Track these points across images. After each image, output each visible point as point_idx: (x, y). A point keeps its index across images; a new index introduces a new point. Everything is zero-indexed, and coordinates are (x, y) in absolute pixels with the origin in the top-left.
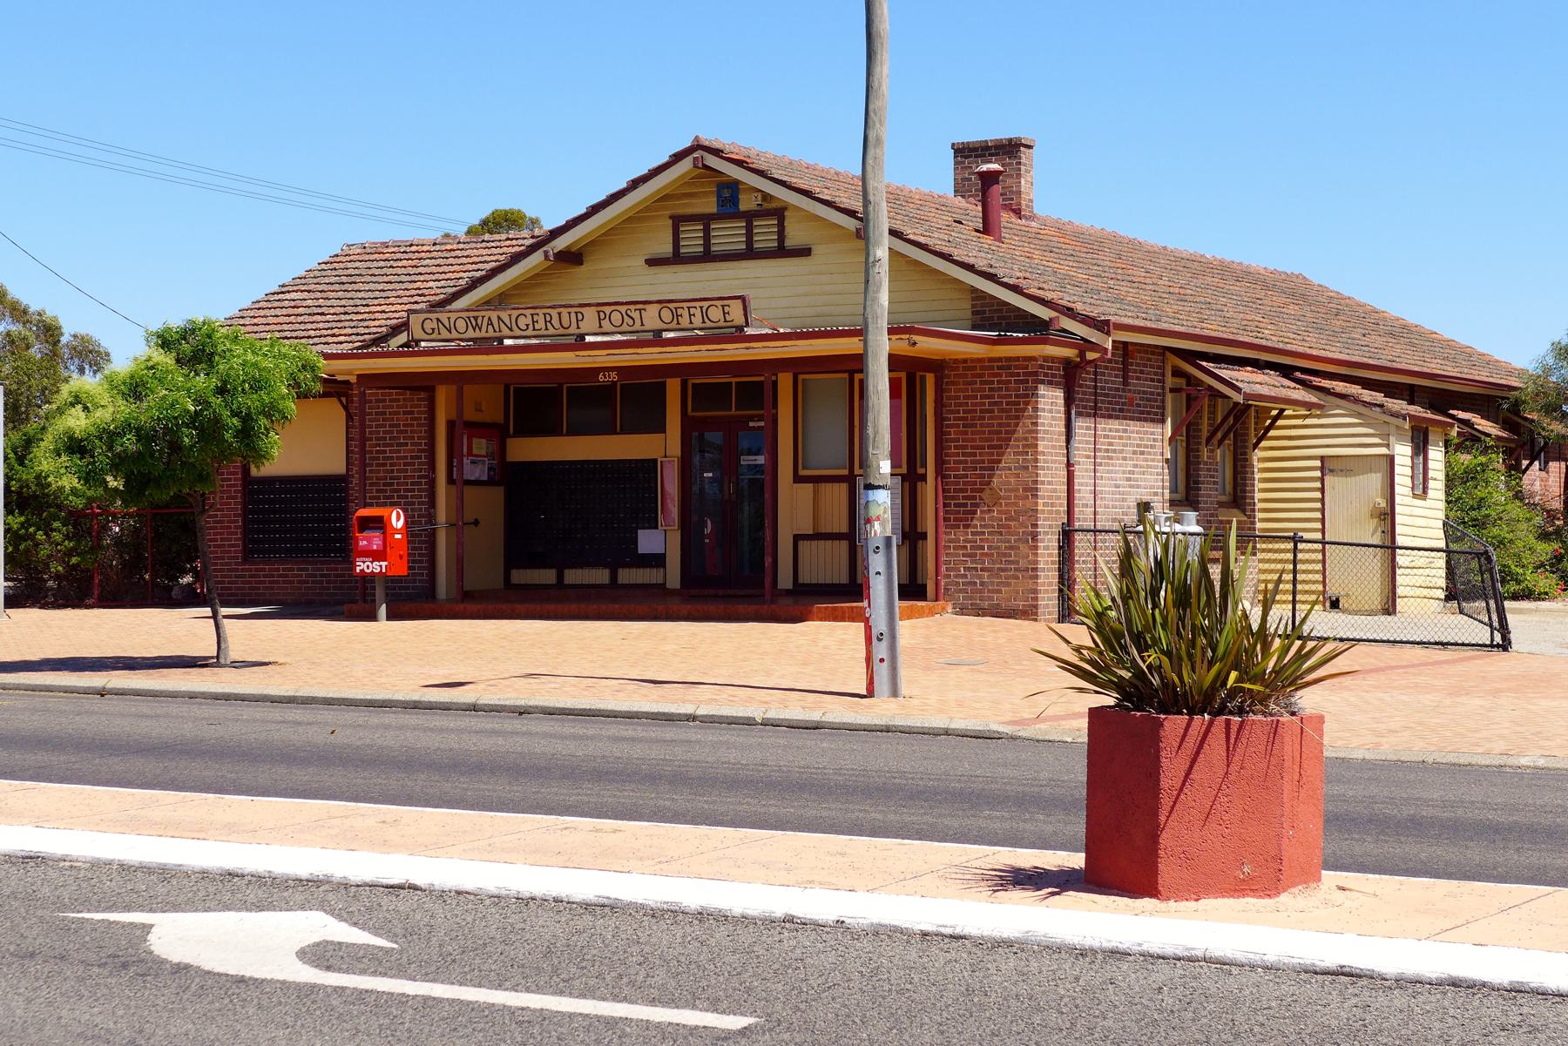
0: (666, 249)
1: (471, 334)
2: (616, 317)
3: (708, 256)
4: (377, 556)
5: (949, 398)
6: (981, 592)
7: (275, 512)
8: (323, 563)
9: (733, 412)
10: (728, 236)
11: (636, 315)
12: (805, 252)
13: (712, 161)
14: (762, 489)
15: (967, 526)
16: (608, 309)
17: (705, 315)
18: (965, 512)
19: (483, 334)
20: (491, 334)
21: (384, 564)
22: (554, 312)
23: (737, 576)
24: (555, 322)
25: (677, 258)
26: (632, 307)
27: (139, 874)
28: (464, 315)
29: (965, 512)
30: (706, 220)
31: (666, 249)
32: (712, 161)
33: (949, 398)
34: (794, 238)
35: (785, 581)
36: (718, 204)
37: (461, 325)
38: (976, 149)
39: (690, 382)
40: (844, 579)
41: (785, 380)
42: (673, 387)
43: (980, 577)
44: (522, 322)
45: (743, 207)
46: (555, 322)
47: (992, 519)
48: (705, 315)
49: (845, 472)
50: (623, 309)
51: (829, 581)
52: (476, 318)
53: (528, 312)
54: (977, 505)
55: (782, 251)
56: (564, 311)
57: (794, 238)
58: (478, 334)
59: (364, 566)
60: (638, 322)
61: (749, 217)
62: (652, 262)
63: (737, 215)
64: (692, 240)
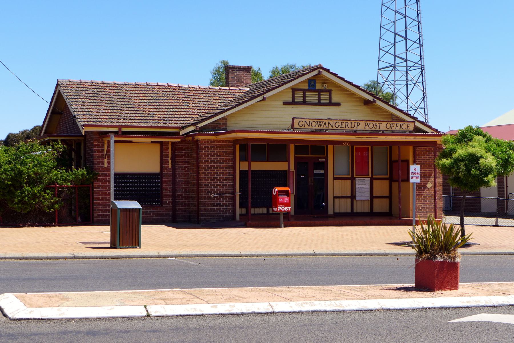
0: (290, 99)
1: (317, 127)
2: (371, 125)
3: (304, 103)
4: (286, 205)
5: (231, 152)
6: (426, 215)
7: (127, 187)
8: (151, 207)
9: (310, 155)
10: (312, 97)
11: (378, 125)
12: (339, 105)
13: (324, 73)
14: (322, 183)
15: (422, 195)
16: (369, 123)
17: (401, 126)
18: (421, 190)
19: (322, 128)
20: (325, 128)
21: (289, 208)
22: (349, 122)
23: (312, 210)
24: (349, 126)
25: (293, 103)
26: (378, 122)
27: (237, 329)
28: (316, 121)
29: (421, 190)
30: (304, 91)
31: (290, 99)
32: (324, 73)
33: (231, 152)
34: (335, 100)
35: (331, 212)
36: (316, 85)
37: (314, 124)
38: (236, 68)
39: (355, 147)
40: (388, 211)
41: (331, 147)
42: (292, 147)
43: (426, 210)
44: (337, 125)
45: (317, 88)
46: (349, 126)
47: (429, 192)
48: (401, 126)
49: (350, 176)
50: (374, 123)
51: (343, 212)
52: (320, 122)
53: (340, 122)
54: (425, 188)
55: (330, 104)
56: (353, 122)
57: (335, 100)
58: (320, 128)
59: (281, 208)
60: (378, 127)
61: (319, 91)
62: (285, 103)
63: (315, 91)
64: (299, 97)
